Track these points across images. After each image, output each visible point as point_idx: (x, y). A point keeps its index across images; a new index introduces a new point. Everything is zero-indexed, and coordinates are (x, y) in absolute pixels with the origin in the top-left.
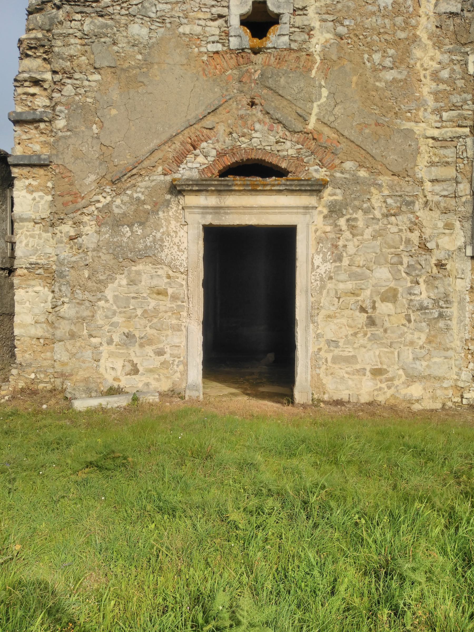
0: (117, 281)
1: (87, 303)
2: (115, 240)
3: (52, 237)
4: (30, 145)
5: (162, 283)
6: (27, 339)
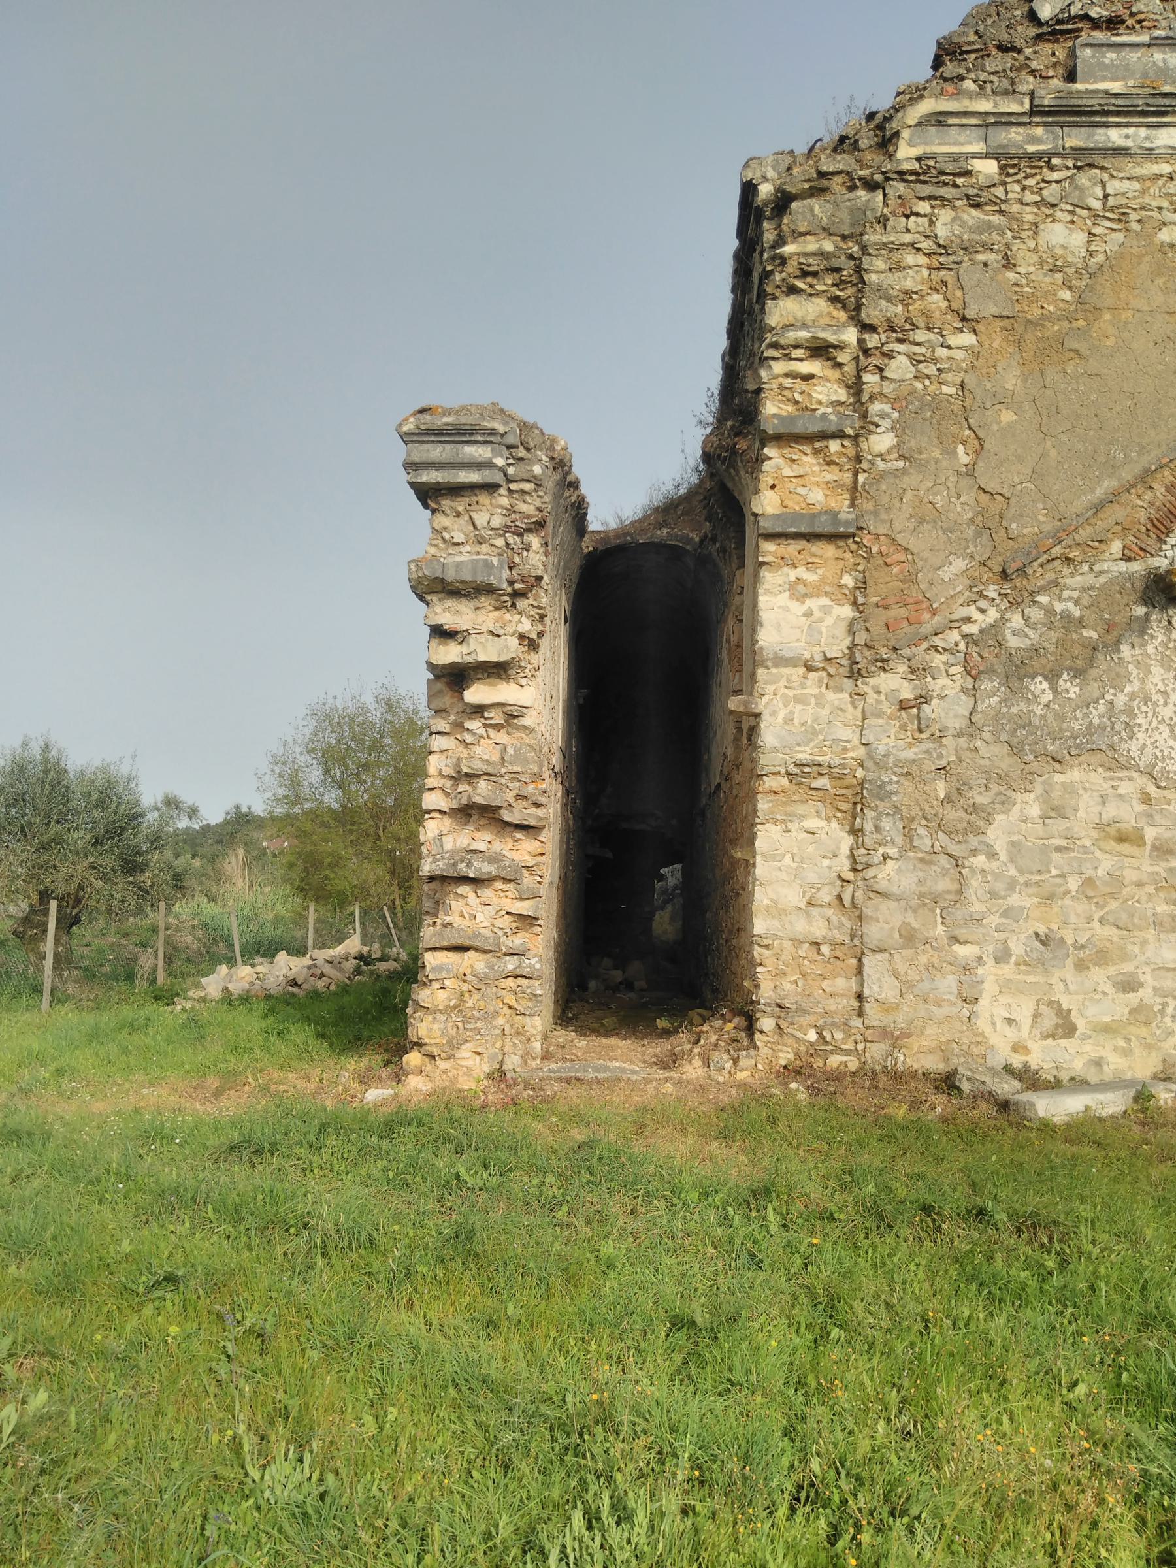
0: (1017, 808)
1: (944, 860)
2: (1014, 710)
3: (853, 703)
4: (801, 490)
5: (1128, 814)
6: (787, 944)
